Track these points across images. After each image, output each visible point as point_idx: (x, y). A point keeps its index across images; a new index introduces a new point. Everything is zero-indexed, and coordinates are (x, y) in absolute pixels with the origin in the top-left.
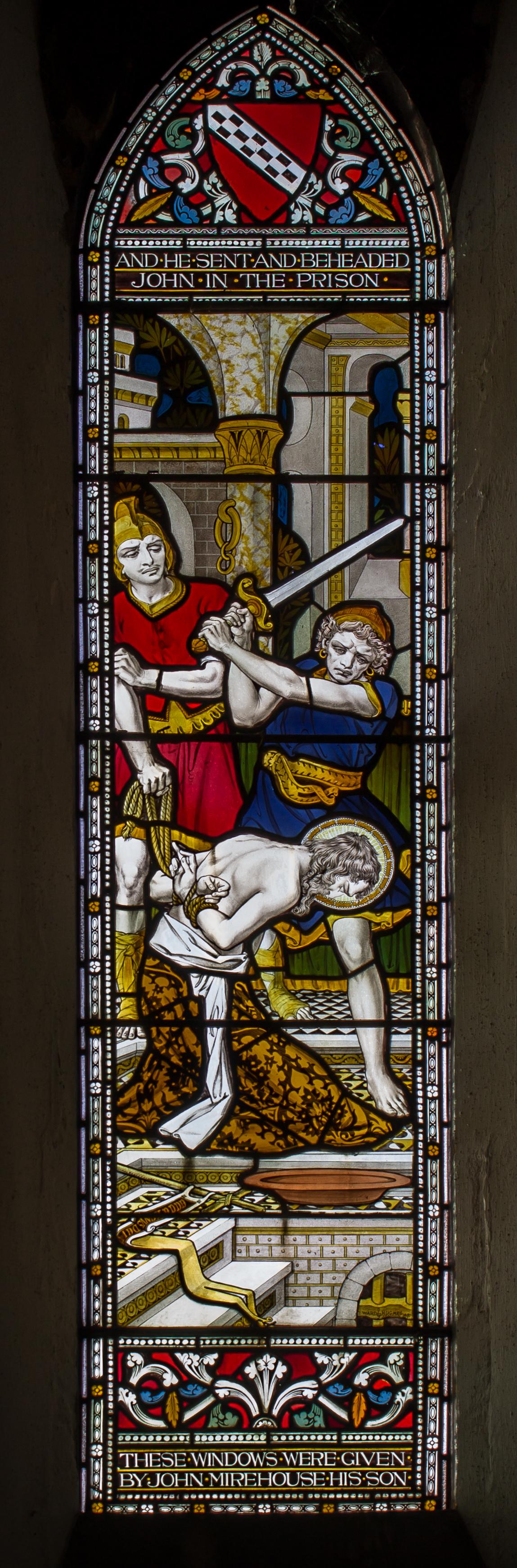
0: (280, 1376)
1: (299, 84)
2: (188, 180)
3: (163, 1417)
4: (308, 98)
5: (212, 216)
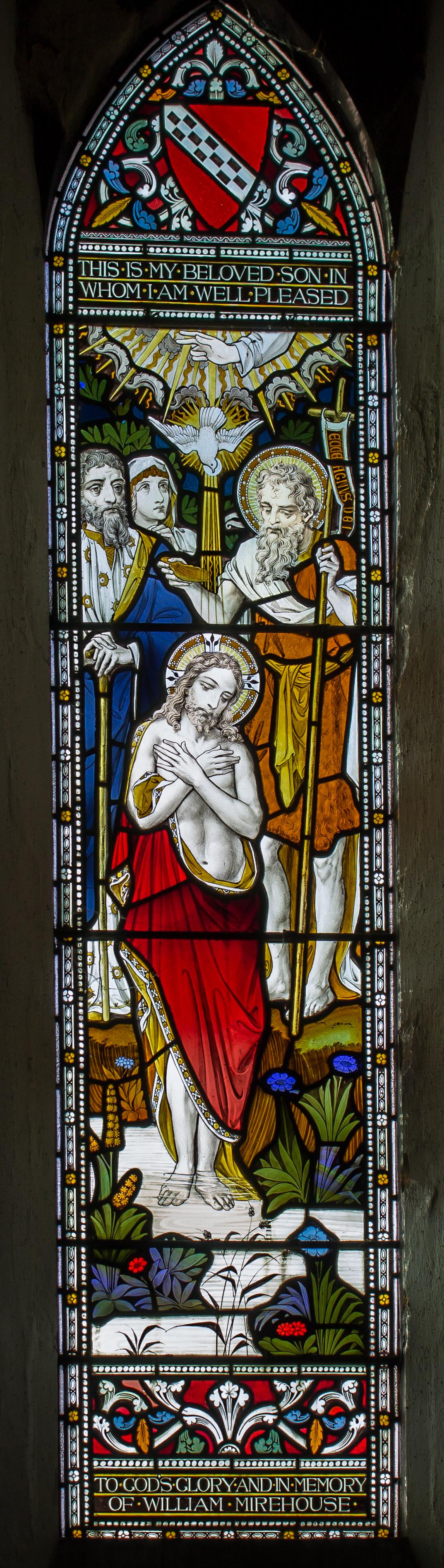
0: (242, 1404)
1: (249, 85)
2: (146, 187)
3: (134, 1443)
4: (256, 99)
5: (169, 221)
